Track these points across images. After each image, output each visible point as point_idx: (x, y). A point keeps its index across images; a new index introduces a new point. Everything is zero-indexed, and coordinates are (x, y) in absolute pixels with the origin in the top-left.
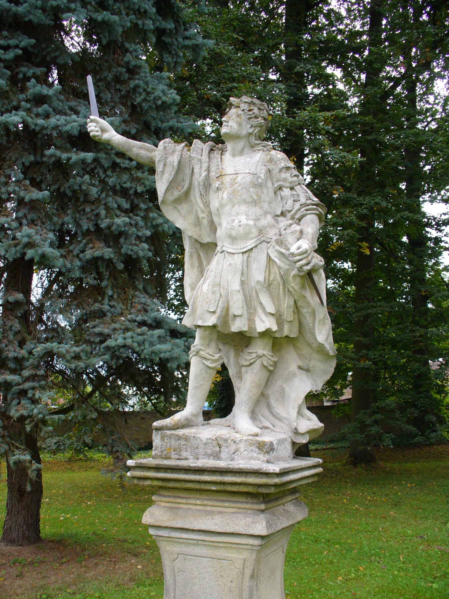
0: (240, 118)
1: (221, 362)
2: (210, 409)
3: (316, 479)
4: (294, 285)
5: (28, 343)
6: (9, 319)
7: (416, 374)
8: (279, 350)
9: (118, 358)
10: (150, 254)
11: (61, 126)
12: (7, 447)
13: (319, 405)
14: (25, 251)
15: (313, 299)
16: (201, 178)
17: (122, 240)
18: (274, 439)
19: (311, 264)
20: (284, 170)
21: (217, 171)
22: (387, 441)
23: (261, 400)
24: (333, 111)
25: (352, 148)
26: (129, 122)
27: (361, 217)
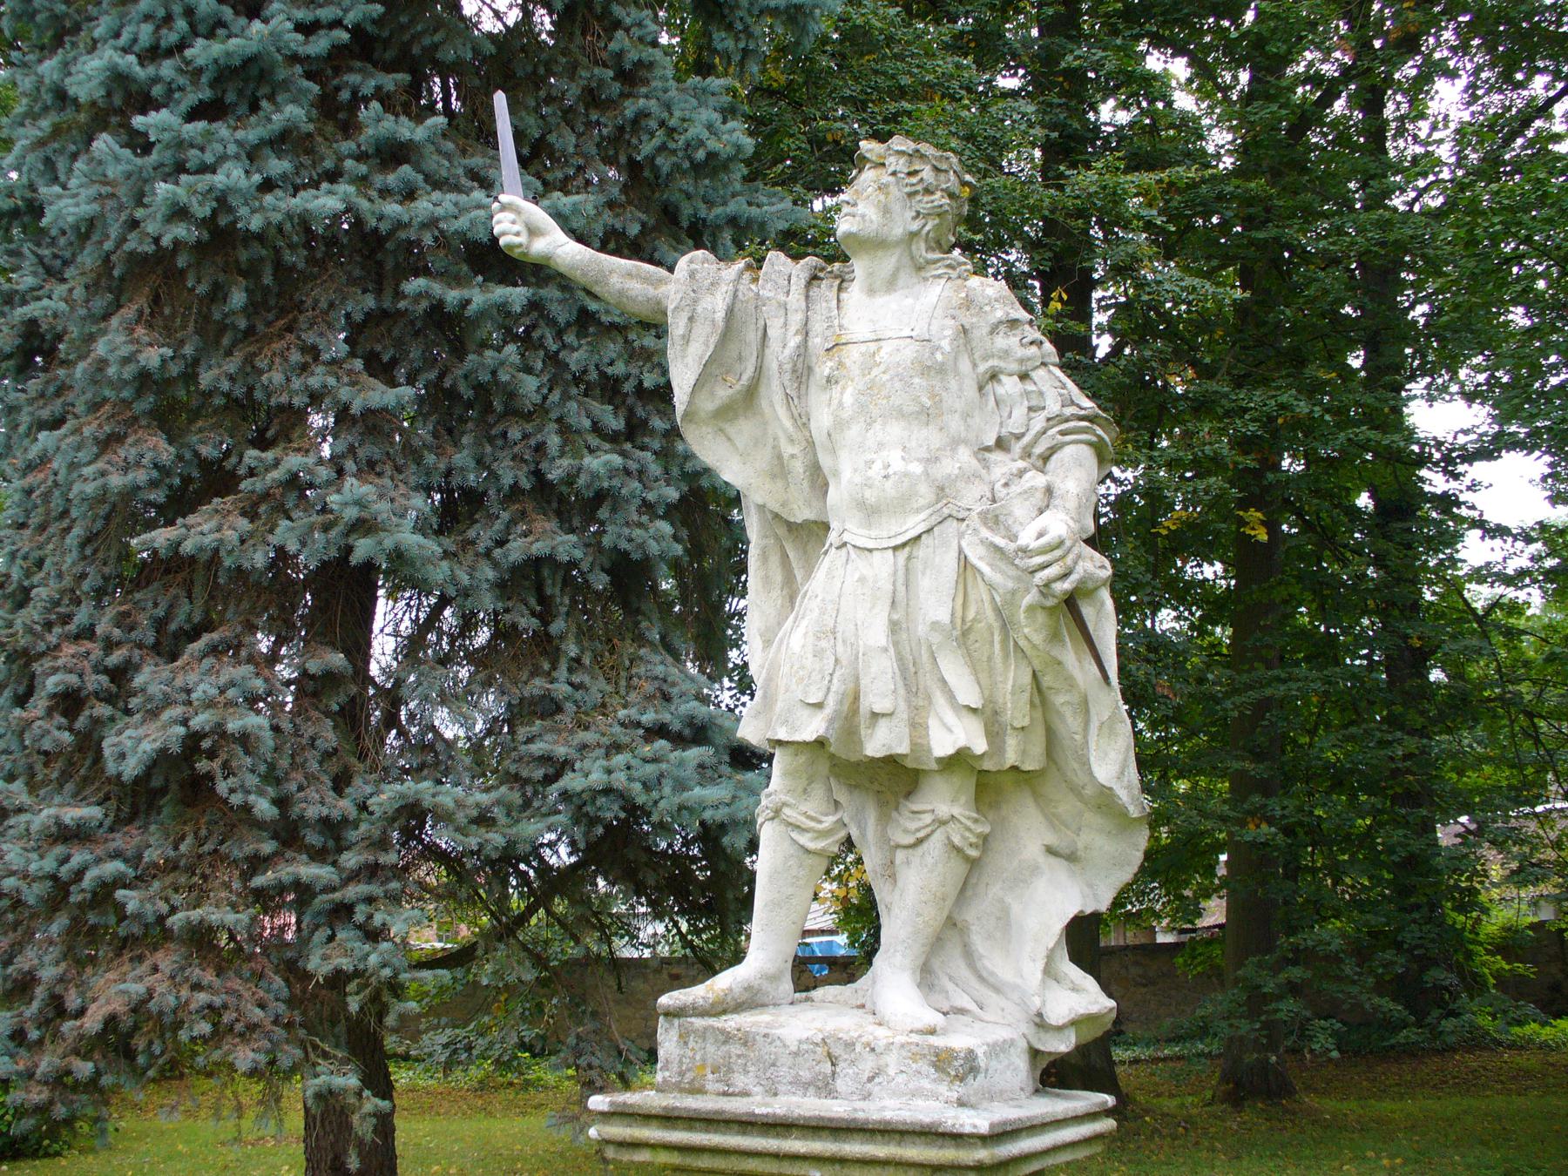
0: (887, 194)
1: (842, 834)
2: (855, 953)
3: (1097, 1148)
4: (1032, 632)
5: (358, 781)
6: (308, 719)
7: (1395, 858)
8: (995, 805)
9: (593, 821)
10: (678, 549)
11: (445, 218)
12: (298, 1053)
13: (1142, 940)
14: (350, 541)
15: (1082, 667)
16: (787, 352)
17: (603, 513)
18: (979, 1041)
19: (1074, 577)
20: (1002, 328)
21: (828, 333)
22: (1323, 1041)
23: (948, 934)
24: (1163, 169)
25: (1215, 263)
26: (621, 206)
27: (1244, 444)
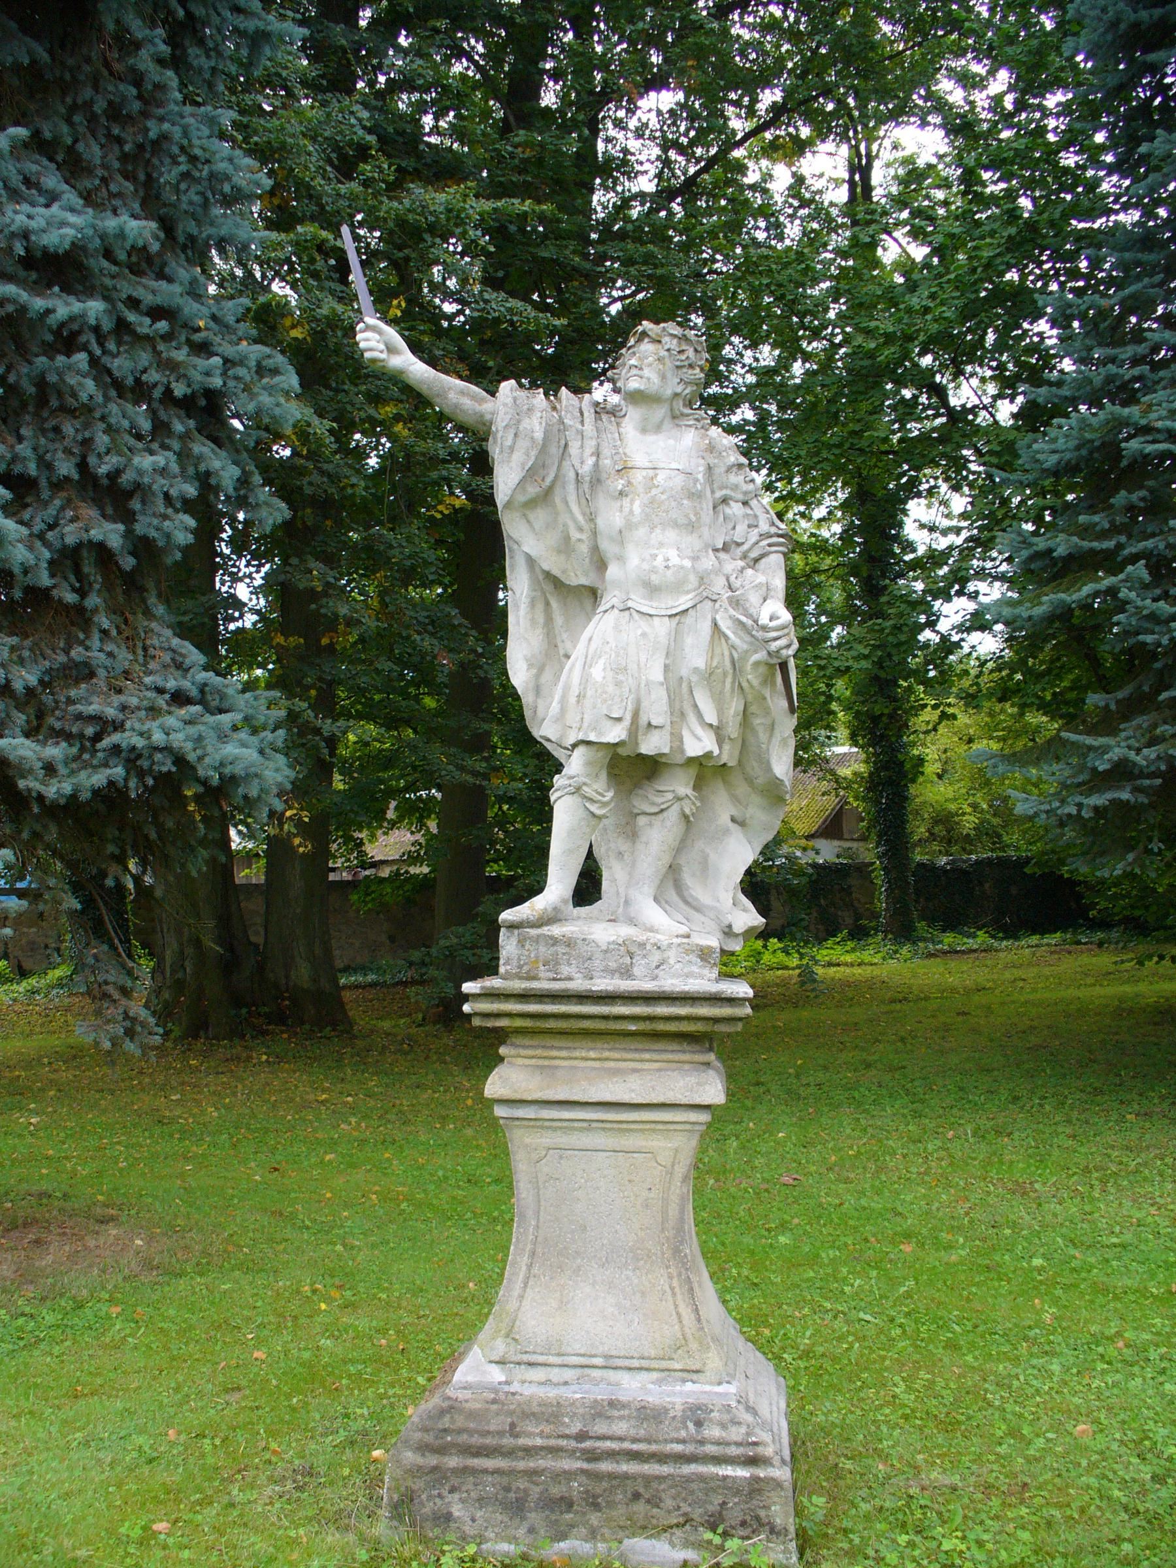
4: (752, 678)
